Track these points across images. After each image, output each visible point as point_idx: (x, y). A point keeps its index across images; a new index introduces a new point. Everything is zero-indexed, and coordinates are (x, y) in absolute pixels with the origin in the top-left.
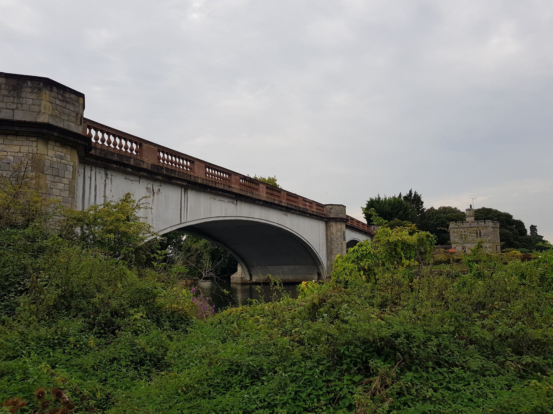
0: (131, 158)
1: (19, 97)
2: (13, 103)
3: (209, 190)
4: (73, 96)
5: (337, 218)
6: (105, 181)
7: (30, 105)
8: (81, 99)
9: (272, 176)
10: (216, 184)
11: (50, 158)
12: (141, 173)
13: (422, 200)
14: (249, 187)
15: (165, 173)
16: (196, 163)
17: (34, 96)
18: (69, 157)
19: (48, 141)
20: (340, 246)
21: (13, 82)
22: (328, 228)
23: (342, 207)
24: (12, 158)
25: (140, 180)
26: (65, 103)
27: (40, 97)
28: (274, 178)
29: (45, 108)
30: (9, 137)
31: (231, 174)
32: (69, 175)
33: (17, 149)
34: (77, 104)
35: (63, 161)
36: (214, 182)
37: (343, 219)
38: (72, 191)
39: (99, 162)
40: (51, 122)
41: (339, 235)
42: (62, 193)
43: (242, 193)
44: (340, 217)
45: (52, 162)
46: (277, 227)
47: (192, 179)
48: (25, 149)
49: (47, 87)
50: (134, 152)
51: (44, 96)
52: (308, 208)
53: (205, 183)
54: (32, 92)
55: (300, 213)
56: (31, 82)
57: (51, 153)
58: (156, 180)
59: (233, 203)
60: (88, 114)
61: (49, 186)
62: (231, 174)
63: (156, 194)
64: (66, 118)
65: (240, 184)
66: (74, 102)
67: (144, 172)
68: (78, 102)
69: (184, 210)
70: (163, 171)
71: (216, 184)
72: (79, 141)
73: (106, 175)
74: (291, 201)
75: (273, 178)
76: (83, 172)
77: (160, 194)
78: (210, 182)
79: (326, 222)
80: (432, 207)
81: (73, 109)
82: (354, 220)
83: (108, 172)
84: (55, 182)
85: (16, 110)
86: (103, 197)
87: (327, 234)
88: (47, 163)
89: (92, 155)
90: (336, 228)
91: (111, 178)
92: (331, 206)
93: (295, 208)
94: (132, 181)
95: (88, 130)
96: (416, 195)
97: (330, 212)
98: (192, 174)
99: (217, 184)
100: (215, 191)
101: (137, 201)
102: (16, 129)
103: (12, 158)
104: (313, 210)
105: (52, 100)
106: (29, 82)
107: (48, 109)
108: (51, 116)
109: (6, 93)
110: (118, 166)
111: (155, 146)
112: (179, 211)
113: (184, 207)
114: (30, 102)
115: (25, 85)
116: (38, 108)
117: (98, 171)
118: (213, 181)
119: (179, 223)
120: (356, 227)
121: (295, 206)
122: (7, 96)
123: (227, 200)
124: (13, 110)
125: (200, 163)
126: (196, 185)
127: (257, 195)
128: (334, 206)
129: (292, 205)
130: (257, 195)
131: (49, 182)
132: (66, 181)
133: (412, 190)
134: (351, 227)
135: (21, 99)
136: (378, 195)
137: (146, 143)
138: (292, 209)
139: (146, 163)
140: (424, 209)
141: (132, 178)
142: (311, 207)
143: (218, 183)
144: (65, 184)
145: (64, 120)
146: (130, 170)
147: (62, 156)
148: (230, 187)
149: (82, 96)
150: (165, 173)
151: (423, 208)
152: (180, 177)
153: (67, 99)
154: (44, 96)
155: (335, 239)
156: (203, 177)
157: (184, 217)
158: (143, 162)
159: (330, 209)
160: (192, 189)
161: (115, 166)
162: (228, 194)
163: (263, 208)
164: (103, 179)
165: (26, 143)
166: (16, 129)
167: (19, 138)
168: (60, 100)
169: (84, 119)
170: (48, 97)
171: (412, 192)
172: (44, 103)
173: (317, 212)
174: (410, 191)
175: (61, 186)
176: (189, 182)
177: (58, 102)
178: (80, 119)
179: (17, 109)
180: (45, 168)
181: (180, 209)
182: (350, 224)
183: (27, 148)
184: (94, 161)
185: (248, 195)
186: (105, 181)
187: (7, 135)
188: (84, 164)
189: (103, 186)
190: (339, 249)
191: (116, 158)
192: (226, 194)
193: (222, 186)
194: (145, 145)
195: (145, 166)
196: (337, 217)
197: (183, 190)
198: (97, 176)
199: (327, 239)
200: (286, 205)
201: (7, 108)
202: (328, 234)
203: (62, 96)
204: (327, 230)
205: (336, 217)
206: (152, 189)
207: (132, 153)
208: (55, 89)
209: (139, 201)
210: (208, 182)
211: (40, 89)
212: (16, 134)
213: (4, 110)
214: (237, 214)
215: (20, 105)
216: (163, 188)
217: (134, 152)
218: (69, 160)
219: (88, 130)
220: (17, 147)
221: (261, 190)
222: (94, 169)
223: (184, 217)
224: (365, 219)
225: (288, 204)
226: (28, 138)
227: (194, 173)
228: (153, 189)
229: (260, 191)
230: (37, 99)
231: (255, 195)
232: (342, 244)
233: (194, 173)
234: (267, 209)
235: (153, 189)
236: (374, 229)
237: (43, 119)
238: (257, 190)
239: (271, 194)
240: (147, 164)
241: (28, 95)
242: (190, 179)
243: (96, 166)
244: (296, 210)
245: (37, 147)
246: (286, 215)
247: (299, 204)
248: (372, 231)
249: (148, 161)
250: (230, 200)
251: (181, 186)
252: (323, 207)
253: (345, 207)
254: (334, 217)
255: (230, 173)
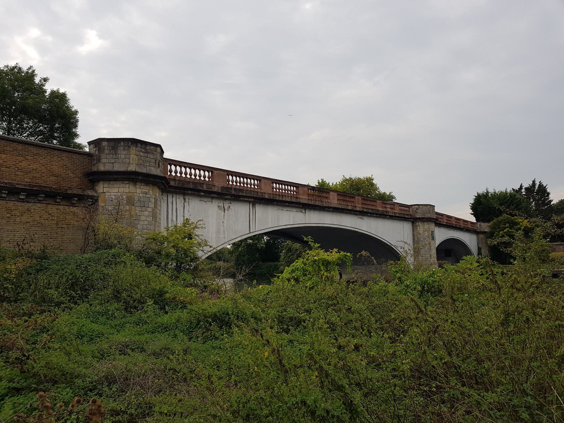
0: (204, 184)
1: (116, 154)
2: (113, 158)
3: (275, 203)
4: (152, 147)
5: (424, 218)
6: (184, 204)
7: (123, 159)
8: (158, 149)
9: (369, 175)
10: (283, 197)
11: (138, 195)
12: (212, 195)
13: (548, 191)
14: (318, 196)
15: (233, 192)
16: (263, 180)
17: (125, 152)
18: (151, 192)
19: (136, 183)
20: (428, 246)
21: (112, 144)
22: (415, 228)
23: (429, 206)
24: (114, 197)
25: (213, 201)
26: (146, 154)
27: (129, 152)
28: (371, 177)
29: (133, 160)
30: (111, 182)
31: (298, 187)
32: (152, 205)
33: (116, 190)
34: (155, 153)
35: (147, 196)
36: (281, 196)
37: (430, 218)
38: (155, 216)
39: (178, 190)
40: (139, 170)
41: (427, 234)
42: (147, 218)
43: (310, 203)
44: (427, 217)
45: (140, 197)
46: (351, 230)
47: (260, 195)
48: (121, 190)
49: (133, 144)
50: (207, 179)
51: (132, 151)
52: (389, 210)
53: (272, 198)
54: (124, 150)
55: (377, 215)
56: (123, 142)
57: (138, 191)
58: (226, 199)
59: (301, 212)
60: (166, 156)
61: (138, 214)
62: (298, 187)
63: (226, 211)
64: (148, 165)
65: (308, 194)
66: (153, 152)
67: (215, 194)
68: (156, 151)
69: (253, 222)
70: (231, 191)
71: (283, 197)
72: (158, 180)
73: (185, 199)
74: (368, 204)
75: (369, 177)
76: (166, 199)
77: (230, 210)
78: (277, 196)
79: (413, 223)
80: (385, 193)
81: (152, 157)
82: (451, 218)
83: (186, 197)
84: (142, 211)
85: (114, 163)
86: (183, 217)
87: (413, 234)
88: (136, 198)
89: (172, 186)
90: (422, 227)
91: (189, 202)
92: (417, 206)
93: (372, 212)
94: (206, 202)
95: (169, 166)
96: (541, 185)
97: (417, 212)
98: (259, 190)
99: (284, 197)
100: (281, 204)
101: (195, 223)
102: (115, 177)
103: (114, 197)
104: (396, 211)
105: (138, 153)
106: (122, 143)
107: (135, 160)
108: (137, 165)
109: (108, 152)
110: (193, 192)
111: (224, 172)
112: (248, 222)
113: (253, 219)
114: (123, 156)
115: (120, 145)
116: (128, 160)
117: (178, 197)
118: (279, 195)
119: (248, 232)
120: (454, 225)
121: (372, 210)
122: (108, 154)
123: (294, 210)
124: (113, 163)
125: (266, 181)
126: (263, 200)
127: (327, 203)
128: (420, 206)
129: (369, 209)
130: (327, 203)
131: (138, 212)
132: (150, 210)
133: (536, 180)
134: (448, 225)
135: (118, 155)
136: (487, 189)
137: (217, 171)
138: (369, 213)
139: (217, 186)
140: (550, 200)
141: (205, 199)
142: (393, 208)
143: (285, 196)
144: (149, 212)
145: (146, 166)
146: (202, 194)
147: (146, 192)
148: (297, 198)
149: (159, 146)
150: (233, 192)
151: (550, 199)
152: (247, 195)
153: (148, 150)
154: (132, 151)
155: (422, 239)
156: (270, 192)
157: (253, 228)
158: (214, 186)
159: (416, 209)
160: (260, 204)
161: (190, 192)
162: (295, 205)
163: (334, 214)
164: (182, 203)
165: (122, 185)
166: (115, 177)
167: (117, 182)
168: (143, 152)
169: (164, 158)
170: (134, 152)
171: (536, 182)
172: (132, 156)
173: (400, 214)
174: (534, 182)
175: (146, 213)
176: (255, 198)
177: (142, 154)
178: (158, 163)
179: (115, 162)
180: (135, 202)
181: (248, 221)
182: (446, 223)
183: (122, 189)
184: (174, 190)
185: (317, 203)
186: (184, 204)
187: (110, 181)
188: (167, 193)
189: (182, 208)
190: (426, 249)
191: (191, 186)
192: (293, 205)
193: (290, 198)
194: (216, 172)
195: (215, 189)
196: (424, 217)
197: (251, 205)
198: (177, 201)
199: (414, 239)
200: (361, 209)
201: (109, 163)
202: (415, 234)
203: (145, 149)
204: (413, 231)
205: (423, 216)
206: (223, 207)
207: (205, 180)
208: (139, 145)
209: (197, 223)
210: (275, 196)
211: (129, 147)
212: (116, 180)
213: (107, 164)
214: (253, 230)
215: (117, 160)
216: (232, 205)
217: (207, 179)
218: (152, 194)
219: (169, 166)
220: (116, 188)
221: (331, 197)
222: (174, 196)
223: (253, 228)
224: (473, 216)
225: (363, 208)
226: (123, 182)
227: (261, 189)
228: (224, 207)
229: (331, 199)
230: (127, 154)
231: (324, 203)
232: (430, 244)
233: (261, 189)
234: (340, 214)
235: (224, 207)
236: (480, 226)
237: (132, 168)
238: (327, 198)
239: (343, 200)
240: (218, 187)
241: (122, 152)
242: (258, 195)
243: (176, 193)
244: (373, 214)
245: (129, 188)
246: (361, 218)
247: (377, 207)
248: (478, 228)
249: (218, 185)
250: (299, 210)
251: (249, 202)
252: (409, 208)
253: (434, 206)
254: (420, 217)
255: (297, 186)
